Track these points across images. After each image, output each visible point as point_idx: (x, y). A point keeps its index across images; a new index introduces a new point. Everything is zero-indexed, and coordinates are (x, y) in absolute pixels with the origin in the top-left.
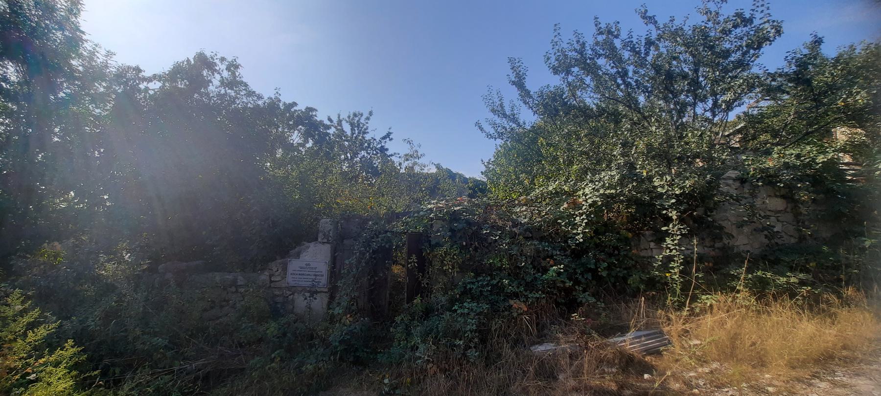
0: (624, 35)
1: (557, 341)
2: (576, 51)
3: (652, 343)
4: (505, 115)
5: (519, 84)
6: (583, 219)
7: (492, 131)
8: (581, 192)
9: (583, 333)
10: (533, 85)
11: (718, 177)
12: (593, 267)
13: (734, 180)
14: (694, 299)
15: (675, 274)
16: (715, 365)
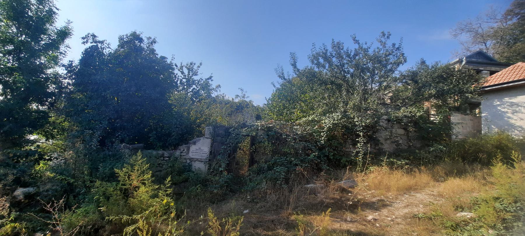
0: (345, 49)
1: (314, 183)
3: (351, 184)
5: (294, 65)
8: (323, 122)
9: (326, 180)
11: (379, 119)
13: (386, 120)
14: (367, 169)
15: (360, 158)
16: (373, 191)
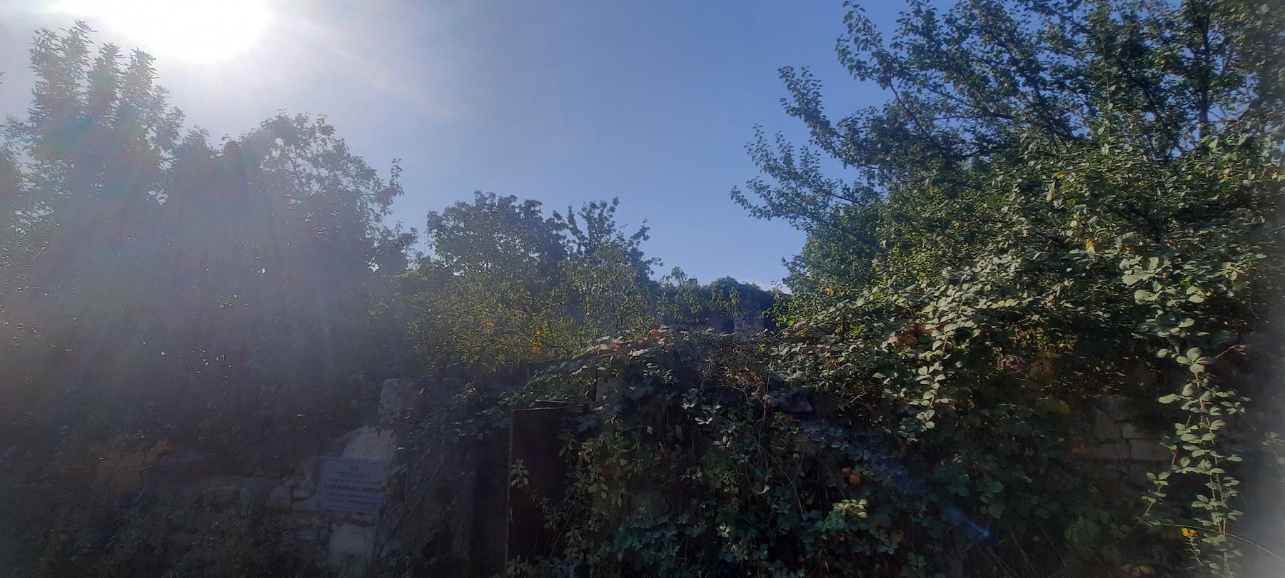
2: (915, 30)
4: (794, 176)
5: (810, 112)
6: (935, 373)
7: (762, 203)
8: (929, 309)
10: (835, 111)
12: (963, 492)
